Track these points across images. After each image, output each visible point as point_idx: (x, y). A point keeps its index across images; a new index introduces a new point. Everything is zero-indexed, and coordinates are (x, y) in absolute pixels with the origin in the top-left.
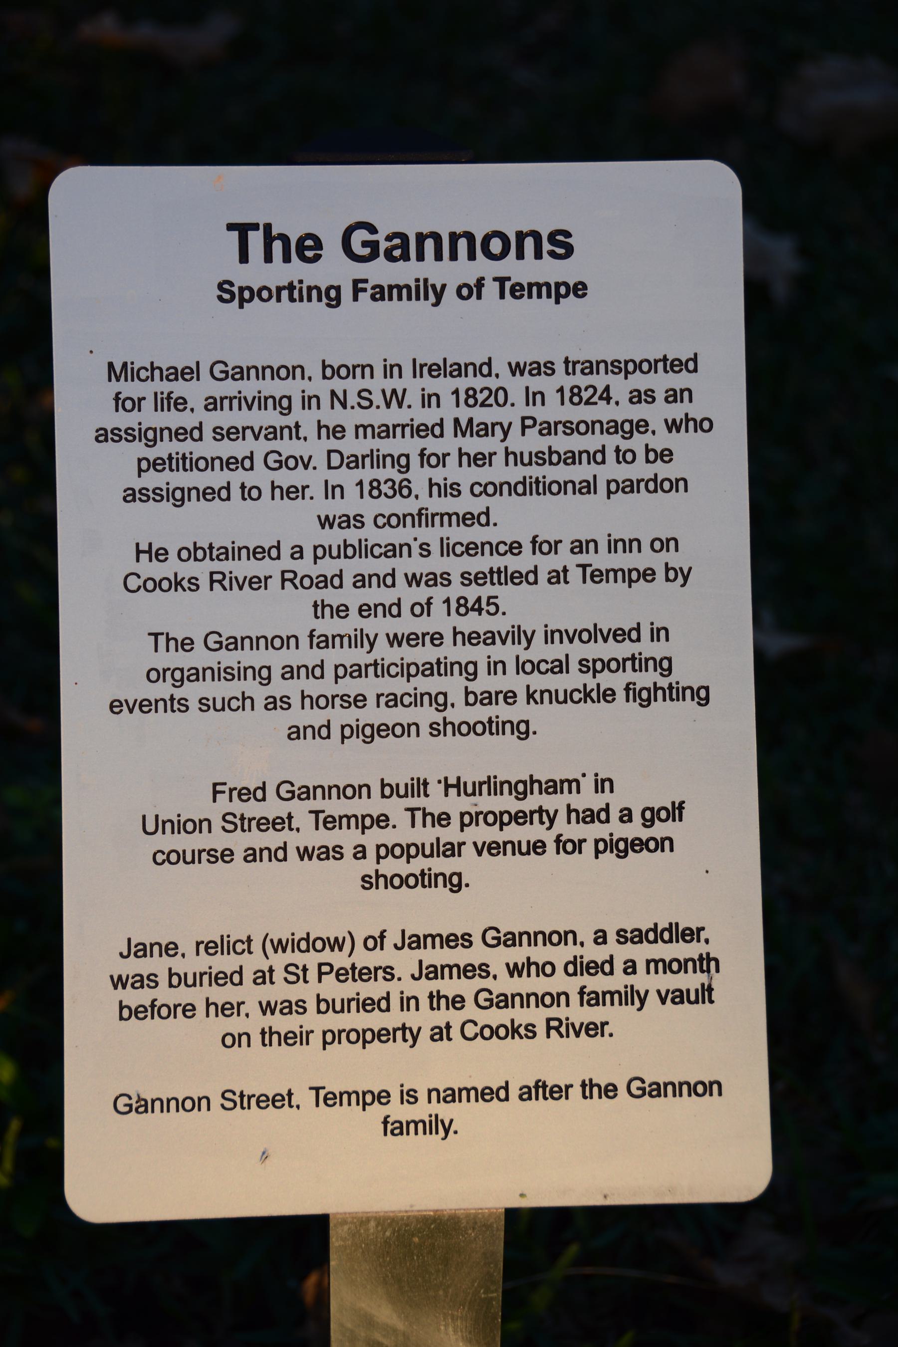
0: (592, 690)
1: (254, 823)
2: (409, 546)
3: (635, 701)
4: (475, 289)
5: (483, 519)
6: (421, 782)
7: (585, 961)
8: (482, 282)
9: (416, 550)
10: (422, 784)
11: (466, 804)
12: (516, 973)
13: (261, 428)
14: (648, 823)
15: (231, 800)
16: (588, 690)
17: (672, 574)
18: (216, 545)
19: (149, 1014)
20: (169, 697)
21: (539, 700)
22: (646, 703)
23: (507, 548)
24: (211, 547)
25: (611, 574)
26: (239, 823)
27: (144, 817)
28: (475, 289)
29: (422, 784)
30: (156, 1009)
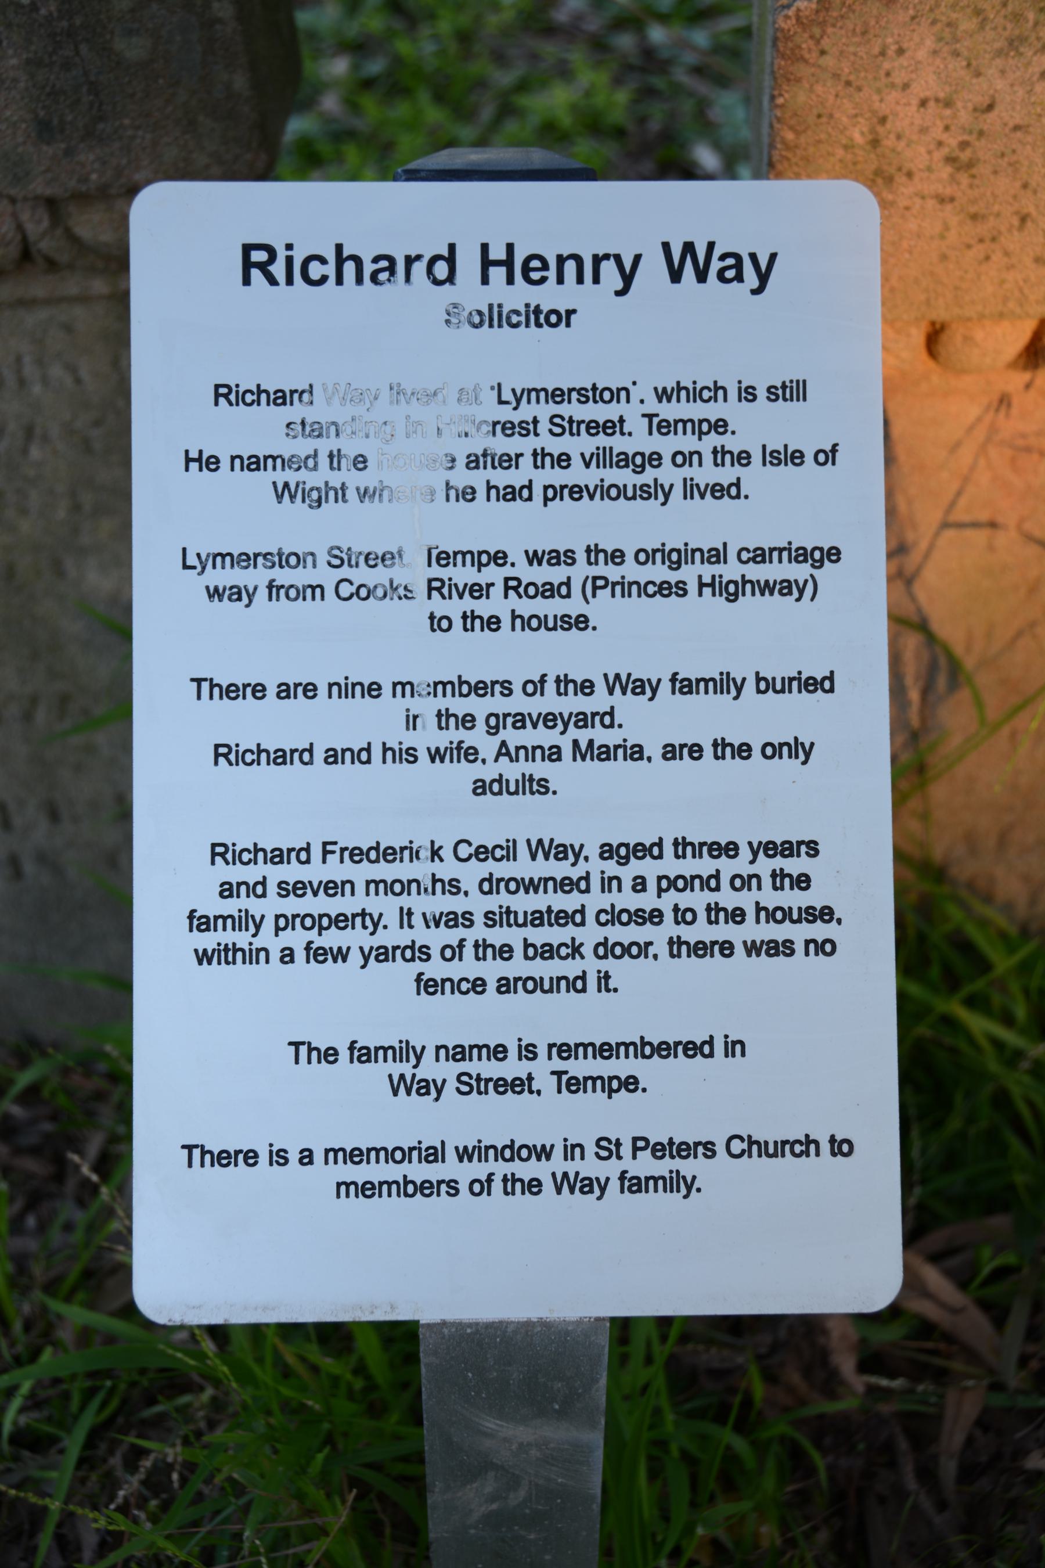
1: (583, 427)
3: (721, 595)
6: (527, 777)
10: (528, 780)
15: (342, 861)
22: (733, 598)
25: (680, 425)
26: (567, 426)
29: (528, 780)
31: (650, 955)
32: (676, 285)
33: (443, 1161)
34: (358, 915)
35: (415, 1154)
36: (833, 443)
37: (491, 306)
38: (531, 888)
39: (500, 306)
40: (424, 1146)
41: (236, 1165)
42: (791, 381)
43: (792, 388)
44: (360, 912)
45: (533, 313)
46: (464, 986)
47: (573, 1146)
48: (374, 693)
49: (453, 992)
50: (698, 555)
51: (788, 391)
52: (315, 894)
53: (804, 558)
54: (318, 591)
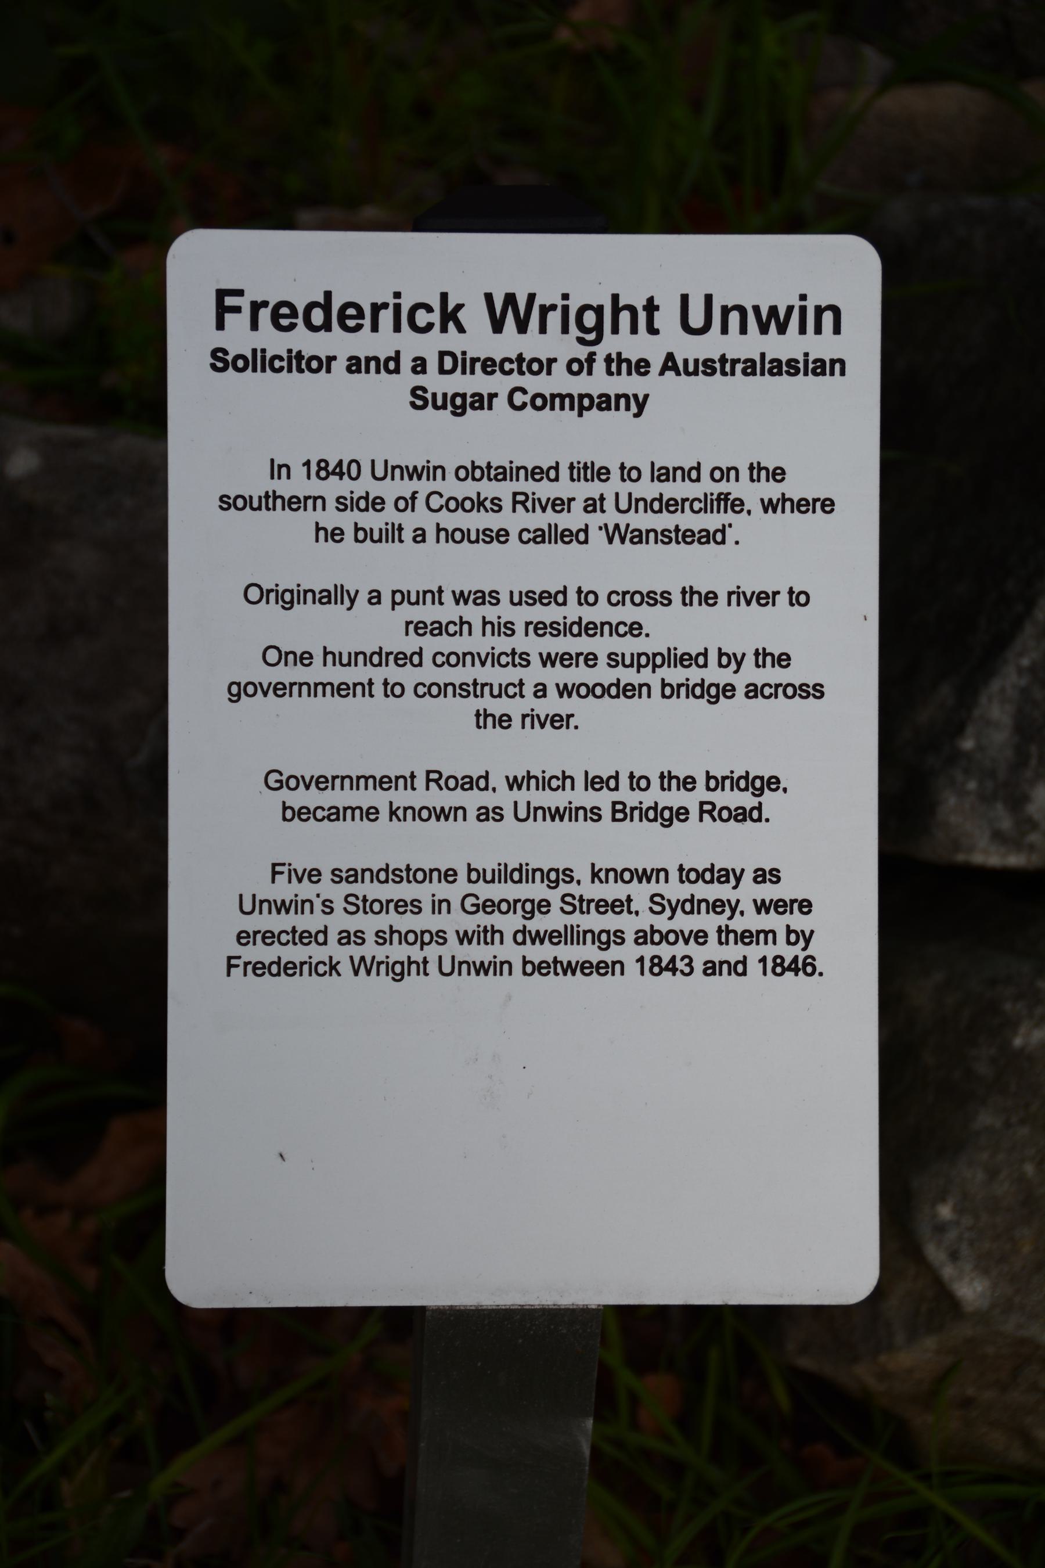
2: (311, 902)
4: (585, 365)
5: (482, 783)
8: (594, 357)
9: (318, 906)
12: (644, 879)
14: (689, 960)
15: (245, 974)
18: (494, 465)
20: (367, 681)
24: (489, 466)
27: (241, 896)
28: (585, 365)
31: (572, 725)
32: (498, 335)
37: (254, 351)
38: (770, 508)
39: (263, 351)
41: (577, 666)
45: (295, 358)
46: (622, 629)
48: (603, 477)
49: (611, 635)
50: (310, 595)
53: (542, 539)
54: (319, 502)
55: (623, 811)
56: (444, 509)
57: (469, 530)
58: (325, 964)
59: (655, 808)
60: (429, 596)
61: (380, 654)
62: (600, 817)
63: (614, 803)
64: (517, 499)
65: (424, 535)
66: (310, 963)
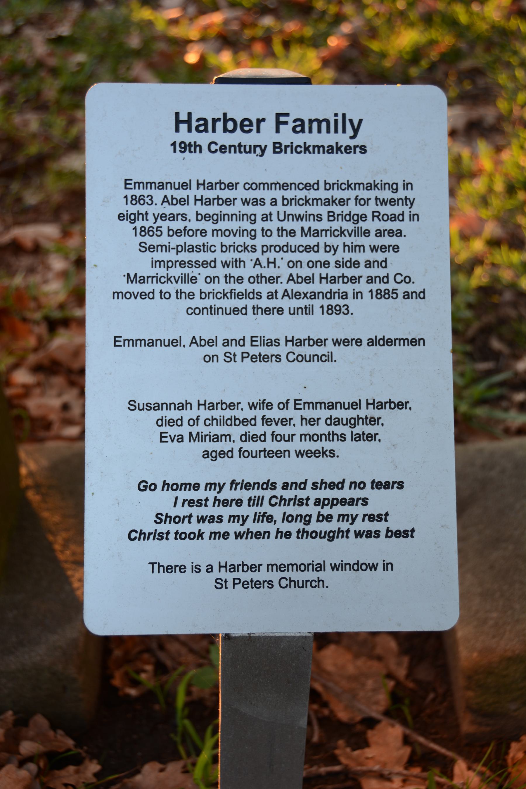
0: (378, 184)
7: (251, 434)
11: (208, 414)
13: (175, 436)
16: (342, 230)
17: (328, 249)
19: (183, 234)
21: (353, 188)
23: (303, 186)
30: (186, 231)
33: (324, 570)
34: (262, 451)
35: (311, 567)
36: (197, 415)
40: (315, 563)
42: (309, 305)
43: (309, 308)
44: (263, 450)
46: (301, 186)
47: (388, 564)
51: (308, 310)
52: (277, 424)
55: (333, 216)
56: (296, 361)
57: (284, 435)
58: (221, 293)
59: (350, 215)
60: (300, 310)
61: (330, 293)
62: (322, 219)
63: (329, 212)
64: (235, 582)
65: (276, 202)
66: (214, 293)
